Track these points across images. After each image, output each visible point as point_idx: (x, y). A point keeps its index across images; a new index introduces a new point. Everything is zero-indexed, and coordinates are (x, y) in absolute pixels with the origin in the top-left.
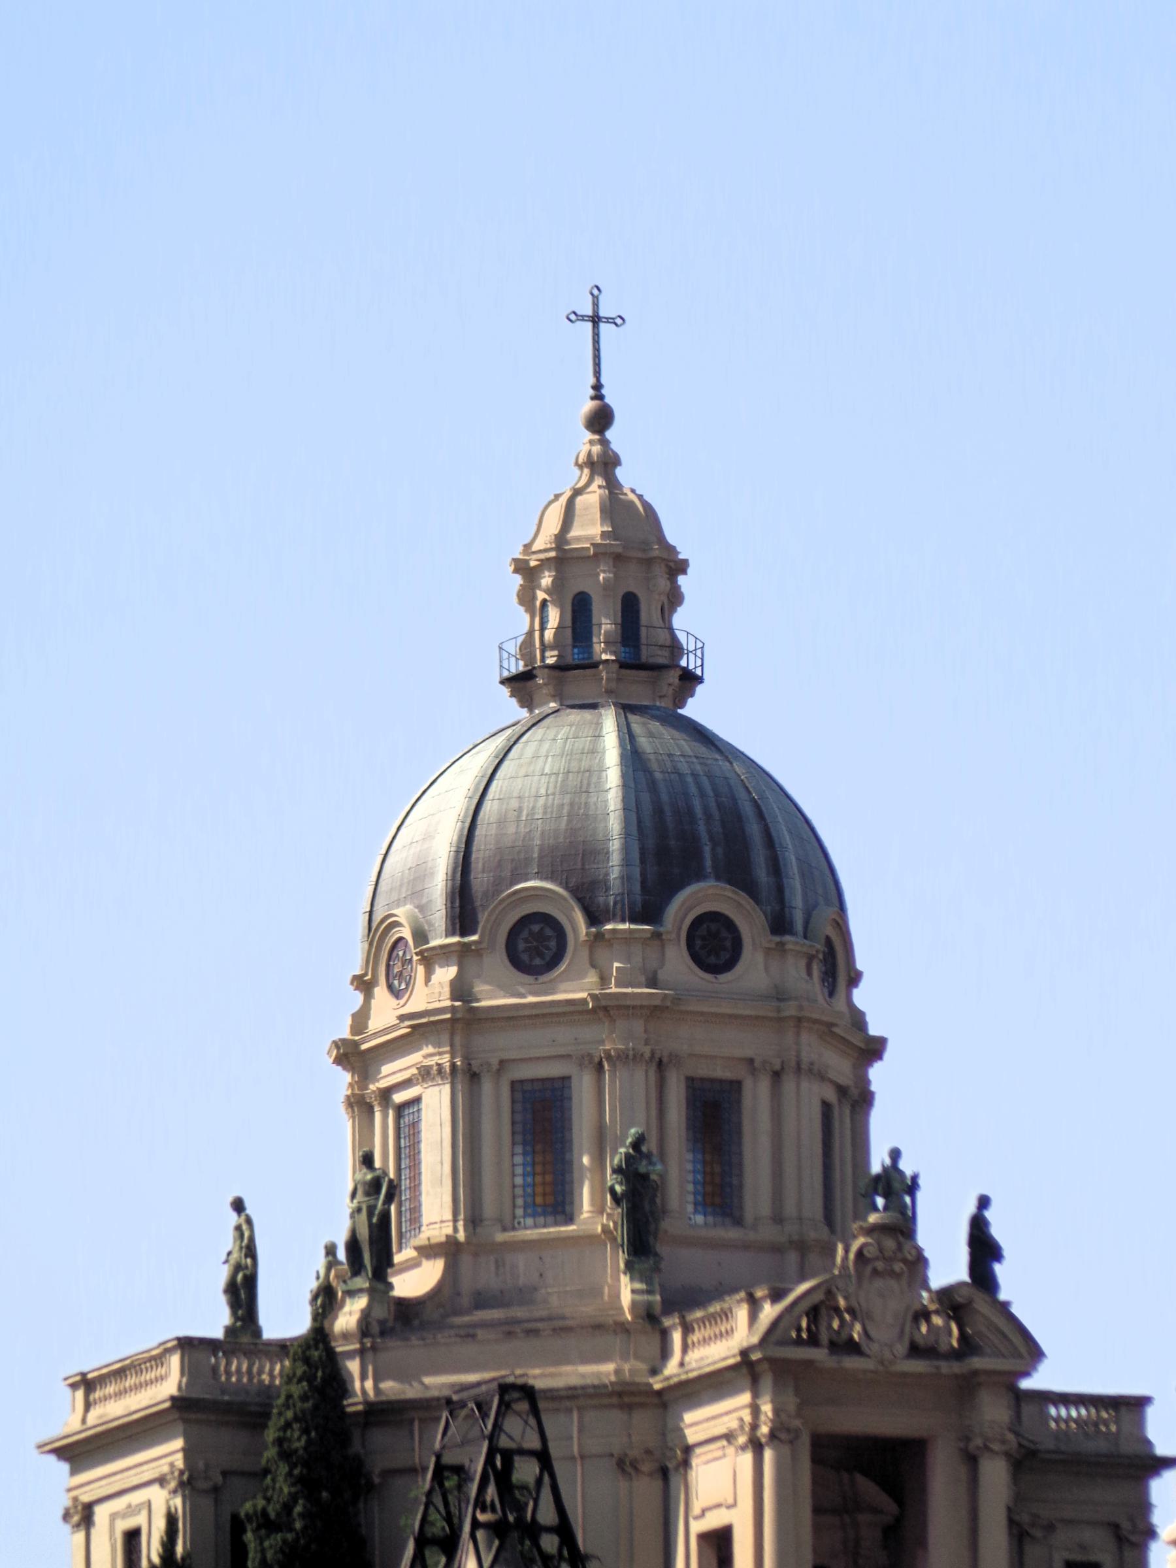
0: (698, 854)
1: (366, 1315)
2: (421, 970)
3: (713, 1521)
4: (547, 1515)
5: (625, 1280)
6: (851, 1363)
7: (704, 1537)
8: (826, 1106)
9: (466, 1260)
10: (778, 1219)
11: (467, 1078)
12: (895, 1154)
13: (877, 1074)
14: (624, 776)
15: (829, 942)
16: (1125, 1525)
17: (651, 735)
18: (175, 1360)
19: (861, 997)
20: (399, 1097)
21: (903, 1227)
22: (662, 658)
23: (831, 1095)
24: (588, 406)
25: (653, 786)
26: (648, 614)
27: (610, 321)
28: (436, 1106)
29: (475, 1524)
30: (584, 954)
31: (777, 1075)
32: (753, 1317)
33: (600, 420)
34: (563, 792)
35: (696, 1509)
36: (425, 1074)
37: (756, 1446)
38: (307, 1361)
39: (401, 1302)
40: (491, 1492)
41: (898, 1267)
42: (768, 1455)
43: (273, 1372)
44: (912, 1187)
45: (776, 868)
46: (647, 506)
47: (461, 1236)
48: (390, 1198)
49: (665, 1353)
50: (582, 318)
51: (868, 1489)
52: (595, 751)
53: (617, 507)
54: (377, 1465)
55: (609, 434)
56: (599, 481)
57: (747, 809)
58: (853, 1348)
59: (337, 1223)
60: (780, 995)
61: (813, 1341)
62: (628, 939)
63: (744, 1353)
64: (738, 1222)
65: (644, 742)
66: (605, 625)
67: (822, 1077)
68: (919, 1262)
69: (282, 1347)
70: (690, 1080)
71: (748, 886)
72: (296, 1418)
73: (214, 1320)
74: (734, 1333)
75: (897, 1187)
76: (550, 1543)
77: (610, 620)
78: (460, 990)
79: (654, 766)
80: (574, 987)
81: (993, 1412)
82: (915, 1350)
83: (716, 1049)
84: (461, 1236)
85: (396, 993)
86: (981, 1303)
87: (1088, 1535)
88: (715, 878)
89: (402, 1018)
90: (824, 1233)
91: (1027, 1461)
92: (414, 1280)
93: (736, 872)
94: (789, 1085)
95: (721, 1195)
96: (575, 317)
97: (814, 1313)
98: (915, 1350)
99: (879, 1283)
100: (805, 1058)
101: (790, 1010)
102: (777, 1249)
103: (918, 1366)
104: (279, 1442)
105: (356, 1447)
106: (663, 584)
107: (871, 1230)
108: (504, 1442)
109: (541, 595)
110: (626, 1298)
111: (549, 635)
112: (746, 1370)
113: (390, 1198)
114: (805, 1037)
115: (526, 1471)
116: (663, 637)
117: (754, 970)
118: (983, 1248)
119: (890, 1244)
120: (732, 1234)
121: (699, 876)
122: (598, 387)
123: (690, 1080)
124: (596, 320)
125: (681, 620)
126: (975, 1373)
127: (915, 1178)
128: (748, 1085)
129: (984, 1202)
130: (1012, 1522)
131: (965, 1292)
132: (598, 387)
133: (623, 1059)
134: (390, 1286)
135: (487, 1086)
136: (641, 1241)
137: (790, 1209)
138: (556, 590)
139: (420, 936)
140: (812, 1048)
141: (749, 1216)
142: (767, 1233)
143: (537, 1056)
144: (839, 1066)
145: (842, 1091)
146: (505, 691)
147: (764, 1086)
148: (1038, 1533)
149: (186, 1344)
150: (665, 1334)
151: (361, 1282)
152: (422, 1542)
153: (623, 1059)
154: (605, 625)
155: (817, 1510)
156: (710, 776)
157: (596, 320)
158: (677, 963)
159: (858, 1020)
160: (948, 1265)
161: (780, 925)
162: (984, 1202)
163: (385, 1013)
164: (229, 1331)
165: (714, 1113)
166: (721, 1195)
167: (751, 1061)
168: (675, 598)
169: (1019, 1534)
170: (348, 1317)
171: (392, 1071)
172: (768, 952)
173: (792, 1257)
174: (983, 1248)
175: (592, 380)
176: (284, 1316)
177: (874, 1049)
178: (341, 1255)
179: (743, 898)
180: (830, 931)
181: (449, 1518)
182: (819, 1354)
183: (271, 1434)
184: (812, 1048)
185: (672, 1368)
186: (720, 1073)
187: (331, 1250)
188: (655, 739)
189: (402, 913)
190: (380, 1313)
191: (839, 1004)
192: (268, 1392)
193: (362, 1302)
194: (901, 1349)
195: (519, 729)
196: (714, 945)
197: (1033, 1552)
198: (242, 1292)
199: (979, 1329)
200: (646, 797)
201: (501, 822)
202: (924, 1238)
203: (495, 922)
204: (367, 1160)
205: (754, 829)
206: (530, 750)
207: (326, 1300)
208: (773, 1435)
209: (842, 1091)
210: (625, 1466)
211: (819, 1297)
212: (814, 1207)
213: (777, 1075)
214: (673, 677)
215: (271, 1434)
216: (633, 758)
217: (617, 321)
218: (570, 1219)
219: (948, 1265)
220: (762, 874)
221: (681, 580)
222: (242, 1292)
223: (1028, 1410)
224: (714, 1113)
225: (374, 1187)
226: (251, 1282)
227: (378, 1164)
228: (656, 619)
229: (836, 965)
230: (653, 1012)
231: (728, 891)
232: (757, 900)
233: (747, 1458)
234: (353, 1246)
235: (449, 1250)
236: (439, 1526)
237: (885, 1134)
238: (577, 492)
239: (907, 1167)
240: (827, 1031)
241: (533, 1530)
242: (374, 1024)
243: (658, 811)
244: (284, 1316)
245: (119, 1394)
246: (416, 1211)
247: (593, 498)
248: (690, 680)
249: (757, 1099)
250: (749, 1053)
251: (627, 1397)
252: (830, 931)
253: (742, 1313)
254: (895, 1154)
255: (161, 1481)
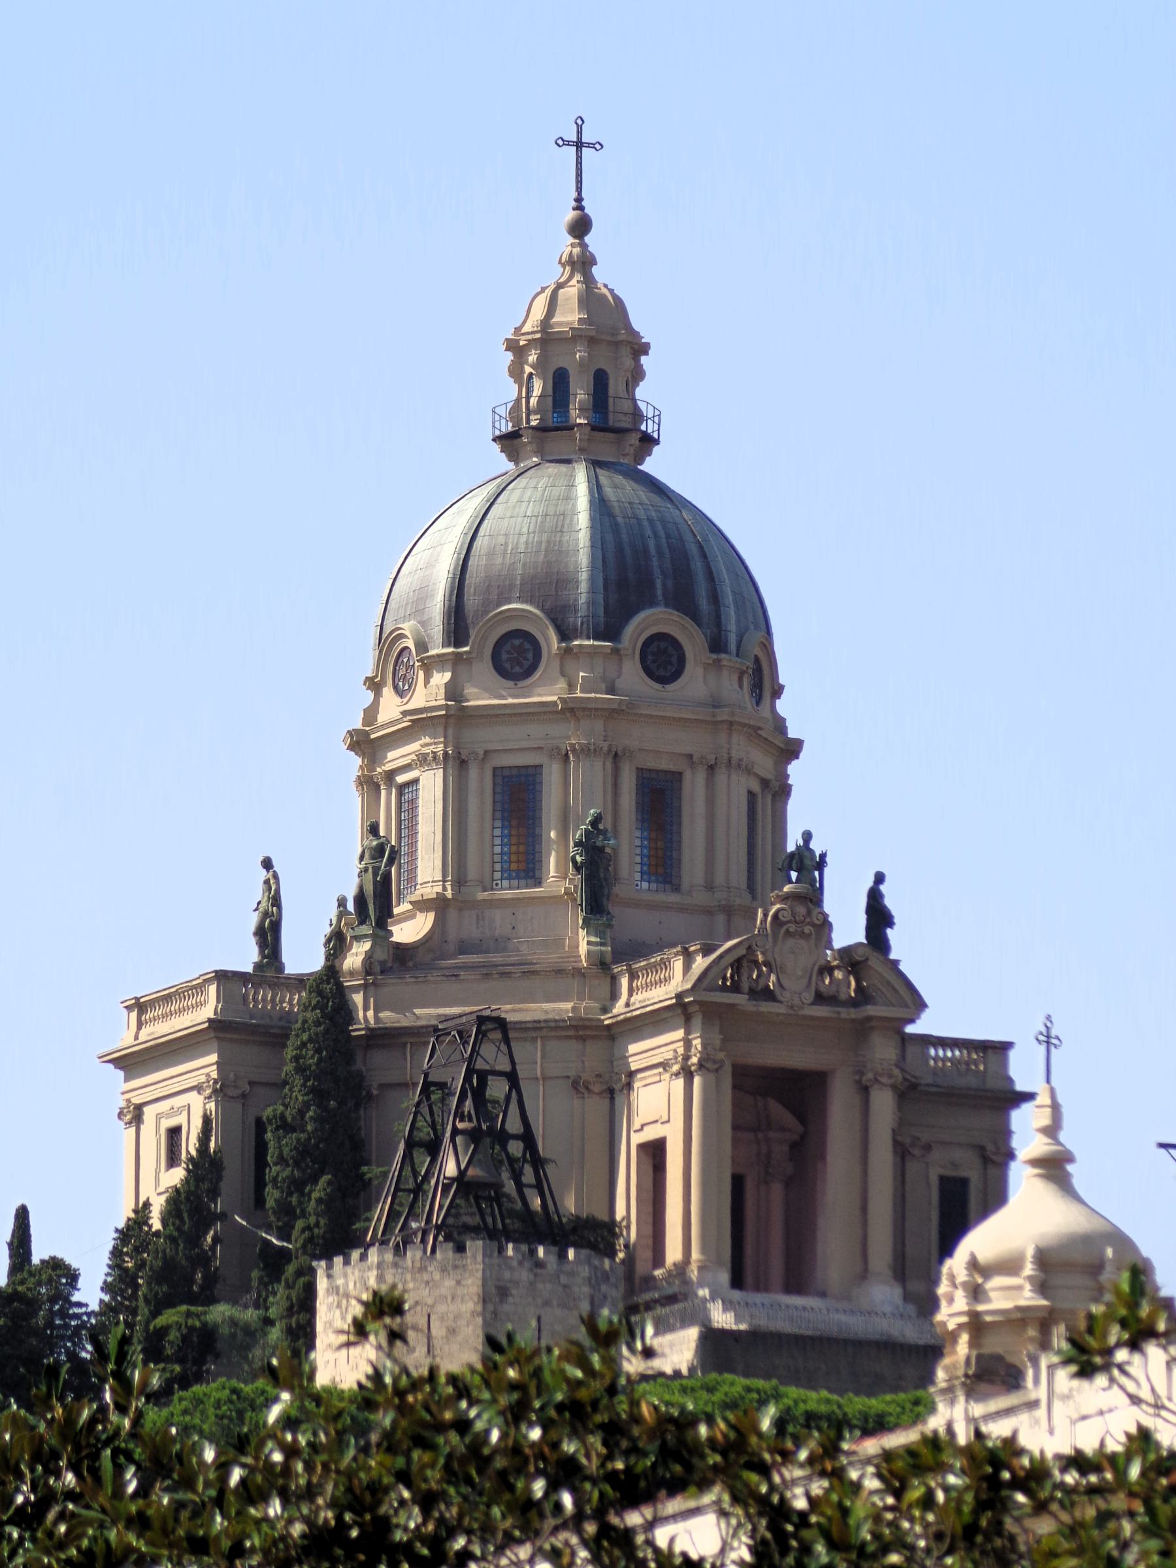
0: (651, 584)
1: (369, 956)
2: (421, 674)
3: (650, 1134)
4: (514, 1125)
5: (582, 933)
6: (766, 1007)
7: (642, 1147)
8: (751, 794)
9: (452, 914)
10: (710, 887)
11: (457, 764)
12: (807, 836)
13: (793, 769)
14: (592, 519)
15: (757, 660)
16: (990, 1147)
17: (615, 486)
18: (213, 989)
19: (782, 706)
20: (401, 779)
21: (813, 897)
22: (625, 423)
23: (756, 787)
24: (570, 215)
25: (615, 528)
26: (615, 386)
27: (590, 145)
28: (431, 787)
29: (455, 1132)
30: (556, 664)
31: (711, 768)
32: (687, 968)
33: (581, 227)
34: (542, 531)
35: (637, 1126)
36: (422, 760)
37: (688, 1075)
38: (320, 993)
39: (398, 945)
40: (468, 1105)
41: (807, 929)
42: (697, 1080)
43: (292, 1002)
44: (821, 864)
45: (715, 598)
46: (617, 299)
47: (449, 894)
48: (391, 861)
49: (614, 996)
50: (567, 143)
51: (777, 1109)
52: (569, 498)
53: (591, 298)
54: (374, 1081)
55: (587, 239)
56: (578, 277)
57: (693, 549)
58: (768, 995)
59: (347, 878)
60: (716, 703)
61: (736, 988)
62: (593, 653)
63: (679, 996)
64: (677, 889)
65: (609, 492)
66: (580, 395)
67: (749, 771)
68: (825, 926)
69: (300, 981)
70: (640, 770)
71: (692, 613)
72: (310, 1040)
73: (245, 957)
74: (674, 979)
75: (808, 863)
76: (516, 1148)
77: (583, 390)
78: (453, 691)
79: (617, 511)
80: (547, 692)
81: (883, 1051)
82: (820, 998)
83: (661, 746)
84: (449, 894)
85: (400, 693)
86: (875, 961)
87: (958, 1155)
88: (669, 601)
89: (405, 713)
90: (746, 899)
91: (910, 1092)
92: (409, 930)
93: (682, 601)
94: (721, 777)
95: (663, 866)
96: (562, 142)
97: (737, 965)
98: (820, 998)
99: (791, 942)
100: (735, 755)
101: (723, 715)
102: (709, 912)
103: (822, 1011)
104: (296, 1058)
105: (359, 1065)
106: (628, 362)
107: (786, 898)
108: (480, 1065)
109: (528, 369)
110: (583, 948)
111: (533, 401)
112: (680, 1011)
113: (391, 861)
114: (735, 738)
115: (497, 1089)
116: (626, 406)
117: (695, 681)
118: (878, 917)
119: (801, 910)
120: (673, 898)
121: (652, 603)
122: (579, 200)
123: (640, 770)
124: (579, 145)
125: (643, 393)
126: (869, 1019)
127: (823, 856)
128: (687, 776)
129: (880, 878)
130: (896, 1143)
131: (861, 951)
132: (579, 200)
133: (585, 752)
134: (391, 934)
135: (473, 772)
136: (597, 902)
137: (720, 879)
138: (540, 365)
139: (422, 646)
140: (740, 747)
141: (685, 884)
142: (700, 898)
143: (515, 747)
144: (763, 763)
145: (765, 783)
146: (496, 447)
147: (701, 777)
148: (916, 1152)
149: (222, 977)
150: (614, 979)
151: (366, 929)
152: (411, 1145)
153: (585, 752)
154: (580, 395)
155: (736, 1127)
156: (663, 521)
157: (579, 145)
158: (632, 676)
159: (780, 725)
160: (848, 928)
161: (717, 645)
162: (880, 878)
163: (391, 708)
164: (258, 966)
165: (659, 798)
166: (663, 866)
167: (690, 756)
168: (638, 375)
169: (902, 1152)
170: (354, 958)
171: (395, 757)
172: (706, 667)
173: (721, 919)
174: (878, 917)
175: (574, 195)
176: (303, 955)
177: (792, 749)
178: (351, 907)
179: (688, 622)
180: (757, 651)
181: (433, 1126)
182: (740, 999)
183: (289, 1053)
184: (740, 747)
185: (619, 1007)
186: (665, 764)
187: (342, 902)
188: (618, 489)
189: (407, 627)
190: (381, 955)
191: (764, 710)
192: (287, 1016)
193: (367, 946)
194: (809, 997)
195: (507, 478)
196: (662, 661)
197: (912, 1167)
198: (269, 935)
199: (873, 981)
200: (610, 537)
201: (491, 554)
202: (830, 905)
203: (482, 637)
204: (374, 830)
205: (697, 565)
206: (517, 493)
207: (337, 943)
208: (701, 1065)
209: (765, 783)
210: (578, 1086)
211: (742, 951)
212: (739, 877)
213: (711, 768)
214: (634, 439)
215: (289, 1053)
216: (599, 504)
217: (597, 146)
218: (539, 883)
219: (848, 928)
220: (704, 603)
221: (643, 359)
222: (269, 935)
223: (912, 1050)
224: (659, 798)
225: (379, 851)
226: (276, 926)
227: (382, 833)
228: (622, 392)
229: (762, 680)
230: (611, 714)
231: (675, 615)
232: (699, 625)
233: (680, 1083)
234: (360, 899)
235: (439, 905)
236: (425, 1133)
237: (805, 816)
238: (560, 286)
239: (817, 846)
240: (754, 733)
241: (502, 1137)
242: (382, 718)
243: (620, 549)
244: (303, 955)
245: (165, 1016)
246: (413, 871)
247: (572, 291)
248: (648, 442)
249: (694, 787)
250: (688, 749)
251: (582, 1031)
252: (757, 651)
253: (678, 964)
254: (807, 836)
255: (198, 1088)
